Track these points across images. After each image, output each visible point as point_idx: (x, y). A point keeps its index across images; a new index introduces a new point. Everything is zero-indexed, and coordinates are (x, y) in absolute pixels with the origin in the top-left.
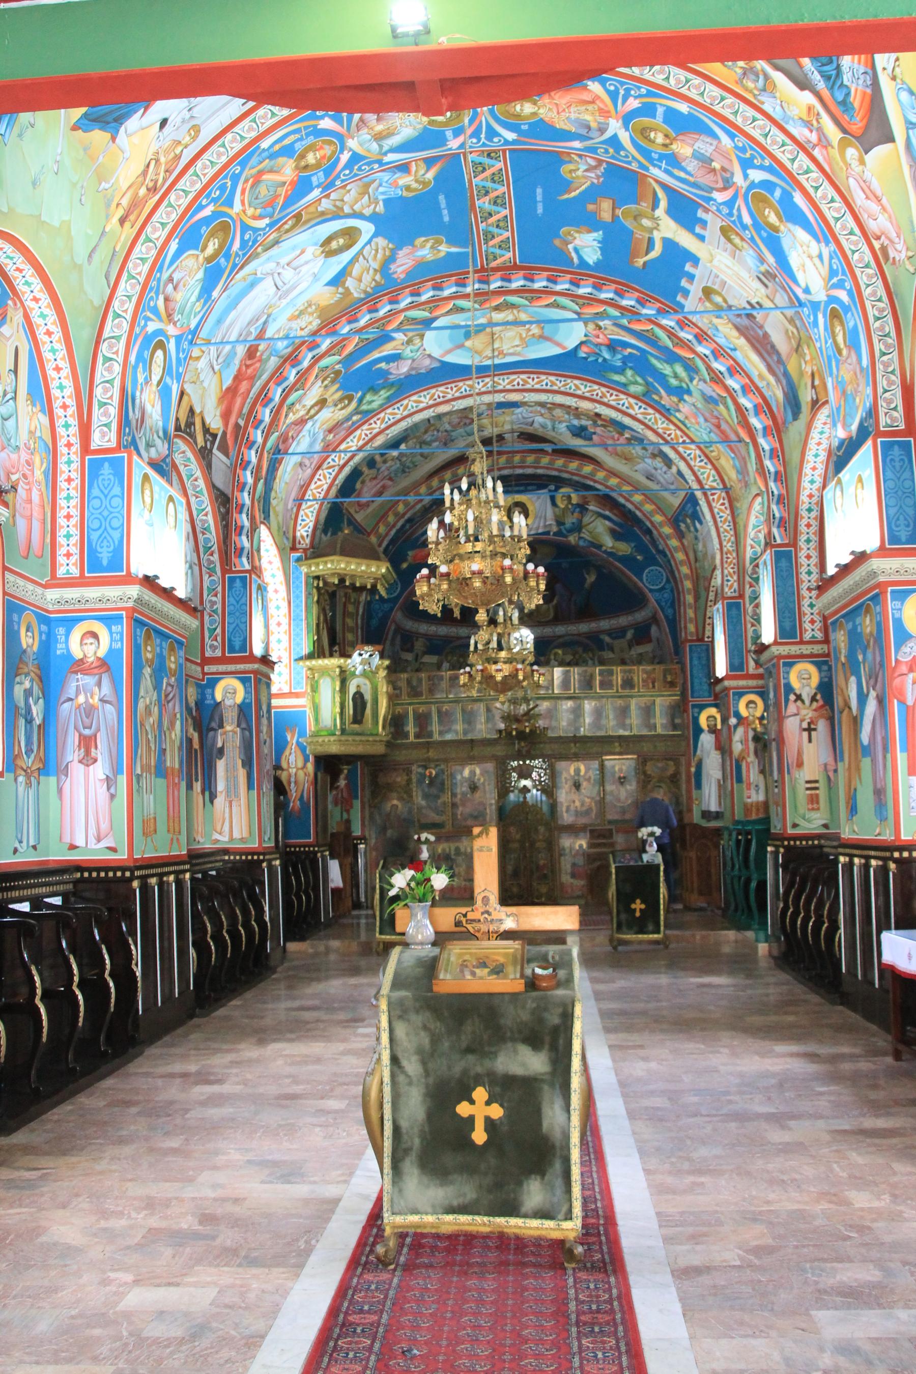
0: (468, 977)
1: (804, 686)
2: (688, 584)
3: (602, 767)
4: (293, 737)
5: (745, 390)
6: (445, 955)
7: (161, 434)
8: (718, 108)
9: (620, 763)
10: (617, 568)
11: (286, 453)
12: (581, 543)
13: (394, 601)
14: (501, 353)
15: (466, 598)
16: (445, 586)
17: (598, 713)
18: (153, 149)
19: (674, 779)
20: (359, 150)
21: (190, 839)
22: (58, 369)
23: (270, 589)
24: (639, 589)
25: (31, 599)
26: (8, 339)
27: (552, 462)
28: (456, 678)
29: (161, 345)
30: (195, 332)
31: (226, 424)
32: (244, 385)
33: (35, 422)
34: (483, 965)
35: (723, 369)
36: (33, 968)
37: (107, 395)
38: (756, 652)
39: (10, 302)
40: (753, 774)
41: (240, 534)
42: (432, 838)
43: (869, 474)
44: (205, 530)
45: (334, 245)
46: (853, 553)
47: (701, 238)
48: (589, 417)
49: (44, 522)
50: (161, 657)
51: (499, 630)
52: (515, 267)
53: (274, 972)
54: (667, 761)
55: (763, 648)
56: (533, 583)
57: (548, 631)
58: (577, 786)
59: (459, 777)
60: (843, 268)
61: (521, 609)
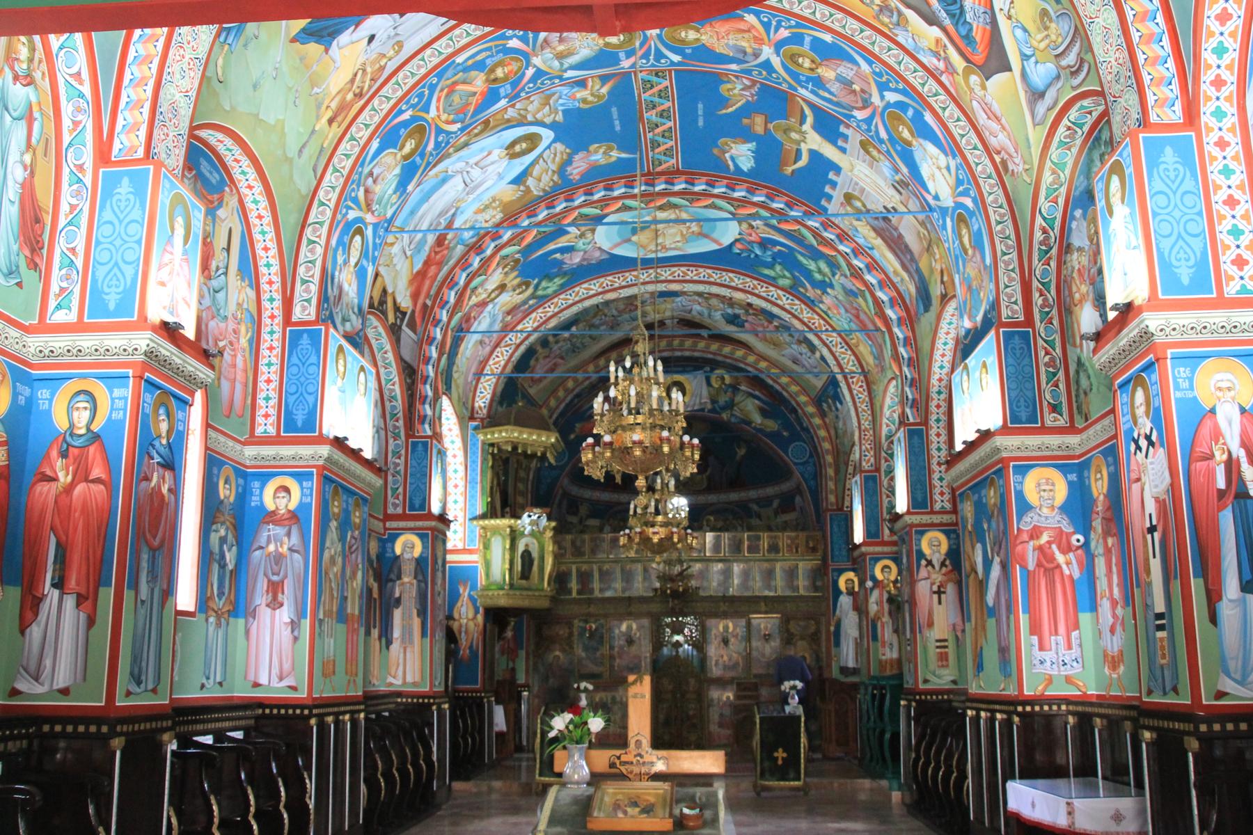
0: (621, 815)
1: (934, 552)
2: (829, 459)
3: (749, 624)
5: (882, 285)
6: (599, 794)
7: (356, 310)
8: (857, 39)
9: (764, 622)
10: (766, 443)
11: (468, 331)
12: (733, 420)
13: (562, 468)
14: (664, 247)
15: (627, 465)
16: (608, 454)
17: (746, 575)
18: (361, 60)
19: (814, 638)
20: (543, 68)
21: (366, 681)
22: (266, 249)
23: (449, 454)
24: (784, 461)
25: (230, 454)
26: (223, 221)
27: (708, 347)
28: (616, 540)
29: (359, 231)
30: (390, 221)
31: (415, 305)
32: (433, 269)
33: (243, 295)
34: (635, 804)
35: (862, 266)
36: (212, 797)
37: (309, 273)
38: (890, 521)
39: (227, 189)
40: (887, 633)
41: (424, 403)
42: (591, 687)
43: (992, 360)
44: (392, 398)
45: (517, 148)
46: (978, 431)
47: (843, 150)
48: (741, 307)
49: (246, 385)
50: (347, 513)
51: (657, 497)
52: (678, 172)
53: (440, 809)
54: (809, 618)
55: (898, 517)
56: (688, 453)
57: (702, 499)
58: (726, 642)
59: (617, 631)
60: (967, 179)
61: (677, 480)
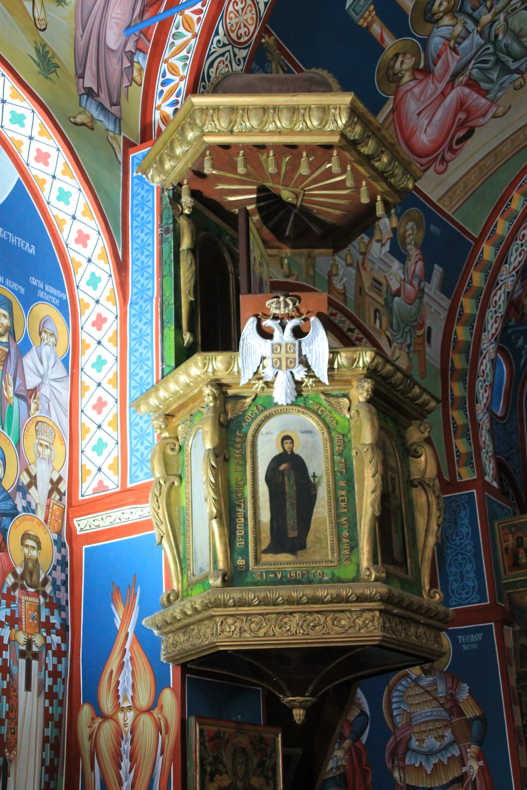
4: (126, 619)
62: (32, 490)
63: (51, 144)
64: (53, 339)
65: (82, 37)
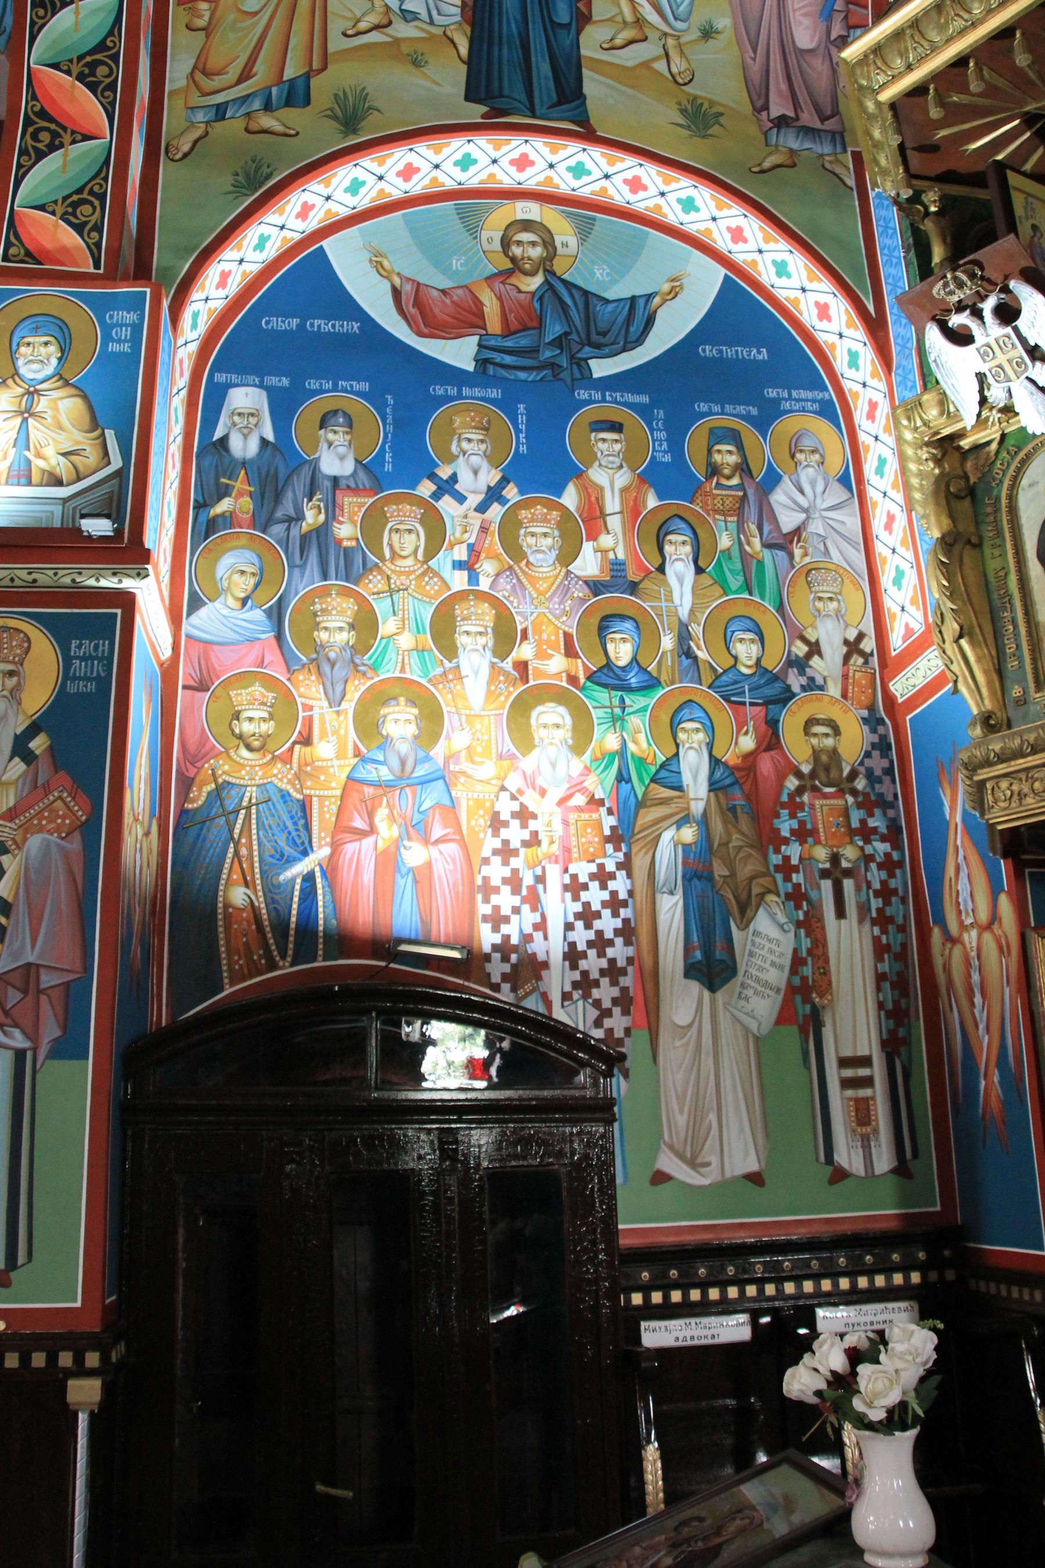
62: (815, 661)
63: (735, 215)
64: (817, 456)
65: (754, 59)
